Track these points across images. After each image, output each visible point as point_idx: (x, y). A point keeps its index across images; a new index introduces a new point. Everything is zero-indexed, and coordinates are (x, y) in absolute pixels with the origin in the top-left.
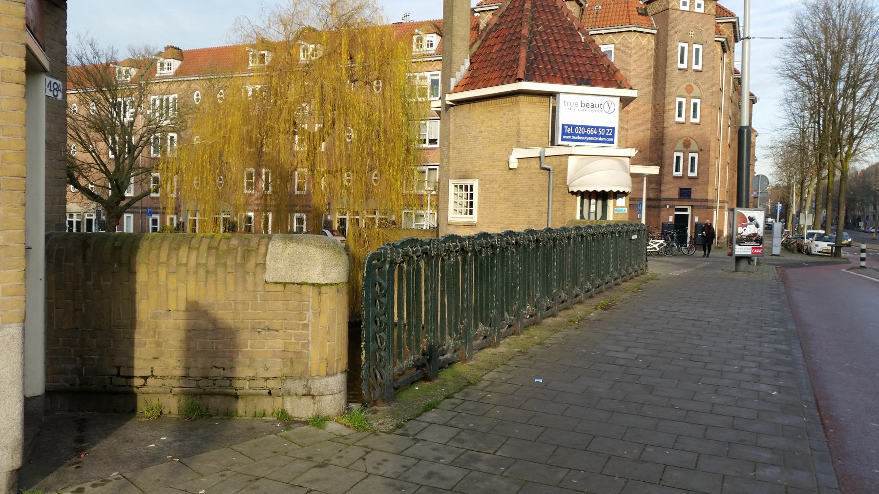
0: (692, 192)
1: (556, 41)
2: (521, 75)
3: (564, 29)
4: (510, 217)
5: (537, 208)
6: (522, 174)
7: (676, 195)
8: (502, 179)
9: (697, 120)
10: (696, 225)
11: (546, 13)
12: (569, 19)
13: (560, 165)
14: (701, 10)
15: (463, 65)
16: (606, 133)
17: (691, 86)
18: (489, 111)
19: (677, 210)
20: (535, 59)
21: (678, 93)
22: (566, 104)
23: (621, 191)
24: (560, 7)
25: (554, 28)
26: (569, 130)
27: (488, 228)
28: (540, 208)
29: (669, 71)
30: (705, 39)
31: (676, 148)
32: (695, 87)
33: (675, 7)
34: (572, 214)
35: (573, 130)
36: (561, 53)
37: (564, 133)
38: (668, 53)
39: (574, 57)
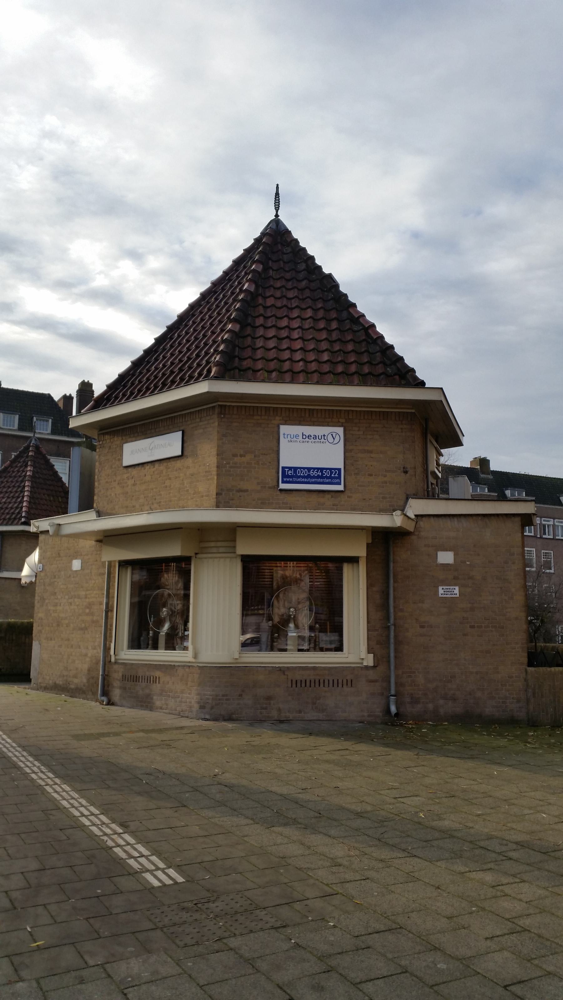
22: (286, 436)
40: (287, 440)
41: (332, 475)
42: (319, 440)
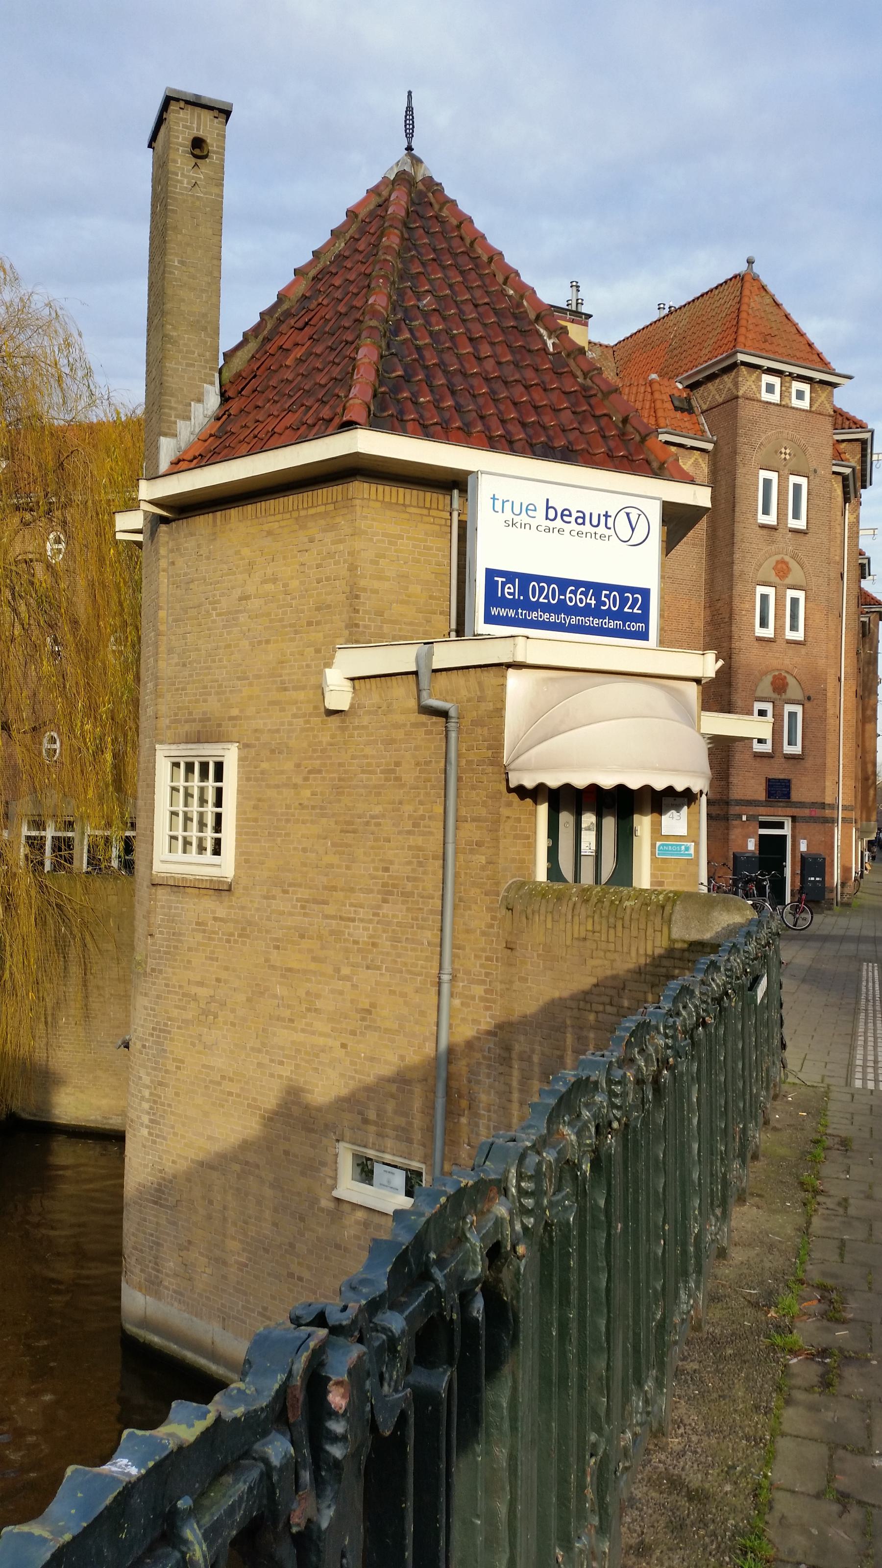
0: (793, 786)
1: (471, 340)
2: (356, 412)
3: (496, 312)
4: (331, 866)
5: (413, 840)
6: (364, 727)
7: (760, 794)
8: (305, 745)
9: (799, 635)
10: (804, 858)
11: (444, 268)
12: (511, 292)
13: (480, 699)
14: (805, 404)
15: (200, 400)
16: (622, 605)
17: (786, 563)
18: (270, 533)
19: (764, 825)
20: (407, 378)
21: (760, 576)
22: (498, 506)
23: (680, 788)
24: (485, 258)
25: (467, 308)
26: (510, 591)
27: (266, 897)
28: (419, 841)
29: (739, 529)
30: (813, 465)
31: (759, 694)
32: (793, 564)
33: (750, 395)
34: (522, 861)
35: (523, 590)
36: (487, 372)
37: (492, 598)
38: (738, 491)
39: (526, 387)
40: (501, 517)
41: (626, 610)
42: (593, 530)
